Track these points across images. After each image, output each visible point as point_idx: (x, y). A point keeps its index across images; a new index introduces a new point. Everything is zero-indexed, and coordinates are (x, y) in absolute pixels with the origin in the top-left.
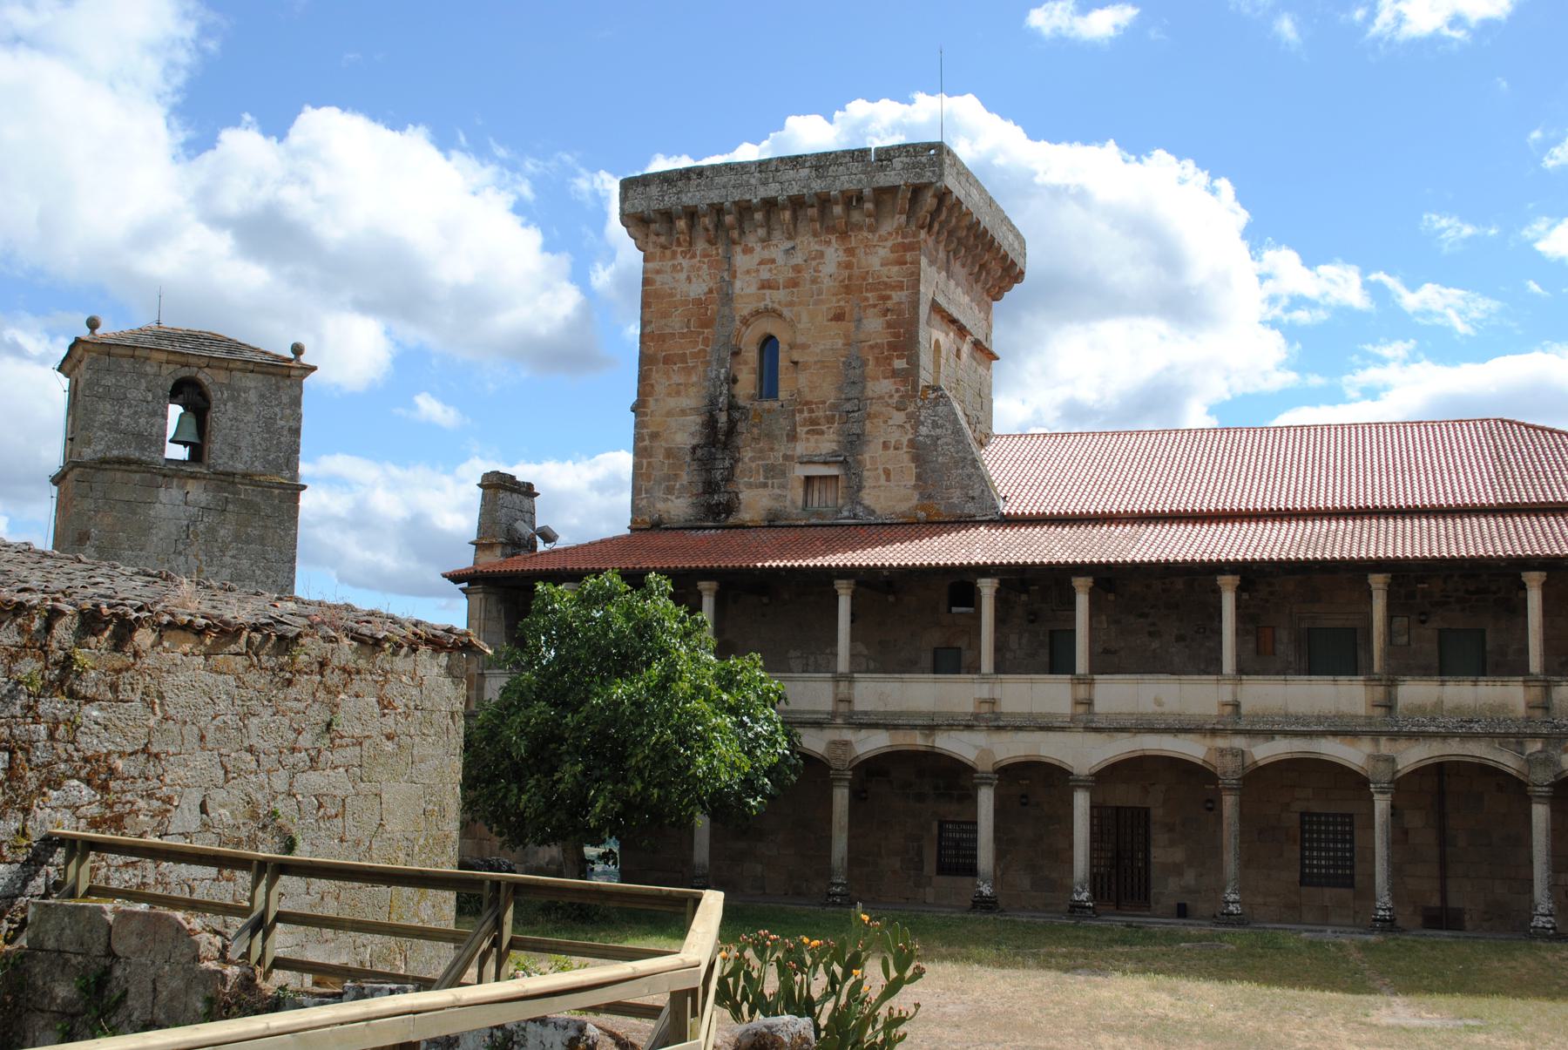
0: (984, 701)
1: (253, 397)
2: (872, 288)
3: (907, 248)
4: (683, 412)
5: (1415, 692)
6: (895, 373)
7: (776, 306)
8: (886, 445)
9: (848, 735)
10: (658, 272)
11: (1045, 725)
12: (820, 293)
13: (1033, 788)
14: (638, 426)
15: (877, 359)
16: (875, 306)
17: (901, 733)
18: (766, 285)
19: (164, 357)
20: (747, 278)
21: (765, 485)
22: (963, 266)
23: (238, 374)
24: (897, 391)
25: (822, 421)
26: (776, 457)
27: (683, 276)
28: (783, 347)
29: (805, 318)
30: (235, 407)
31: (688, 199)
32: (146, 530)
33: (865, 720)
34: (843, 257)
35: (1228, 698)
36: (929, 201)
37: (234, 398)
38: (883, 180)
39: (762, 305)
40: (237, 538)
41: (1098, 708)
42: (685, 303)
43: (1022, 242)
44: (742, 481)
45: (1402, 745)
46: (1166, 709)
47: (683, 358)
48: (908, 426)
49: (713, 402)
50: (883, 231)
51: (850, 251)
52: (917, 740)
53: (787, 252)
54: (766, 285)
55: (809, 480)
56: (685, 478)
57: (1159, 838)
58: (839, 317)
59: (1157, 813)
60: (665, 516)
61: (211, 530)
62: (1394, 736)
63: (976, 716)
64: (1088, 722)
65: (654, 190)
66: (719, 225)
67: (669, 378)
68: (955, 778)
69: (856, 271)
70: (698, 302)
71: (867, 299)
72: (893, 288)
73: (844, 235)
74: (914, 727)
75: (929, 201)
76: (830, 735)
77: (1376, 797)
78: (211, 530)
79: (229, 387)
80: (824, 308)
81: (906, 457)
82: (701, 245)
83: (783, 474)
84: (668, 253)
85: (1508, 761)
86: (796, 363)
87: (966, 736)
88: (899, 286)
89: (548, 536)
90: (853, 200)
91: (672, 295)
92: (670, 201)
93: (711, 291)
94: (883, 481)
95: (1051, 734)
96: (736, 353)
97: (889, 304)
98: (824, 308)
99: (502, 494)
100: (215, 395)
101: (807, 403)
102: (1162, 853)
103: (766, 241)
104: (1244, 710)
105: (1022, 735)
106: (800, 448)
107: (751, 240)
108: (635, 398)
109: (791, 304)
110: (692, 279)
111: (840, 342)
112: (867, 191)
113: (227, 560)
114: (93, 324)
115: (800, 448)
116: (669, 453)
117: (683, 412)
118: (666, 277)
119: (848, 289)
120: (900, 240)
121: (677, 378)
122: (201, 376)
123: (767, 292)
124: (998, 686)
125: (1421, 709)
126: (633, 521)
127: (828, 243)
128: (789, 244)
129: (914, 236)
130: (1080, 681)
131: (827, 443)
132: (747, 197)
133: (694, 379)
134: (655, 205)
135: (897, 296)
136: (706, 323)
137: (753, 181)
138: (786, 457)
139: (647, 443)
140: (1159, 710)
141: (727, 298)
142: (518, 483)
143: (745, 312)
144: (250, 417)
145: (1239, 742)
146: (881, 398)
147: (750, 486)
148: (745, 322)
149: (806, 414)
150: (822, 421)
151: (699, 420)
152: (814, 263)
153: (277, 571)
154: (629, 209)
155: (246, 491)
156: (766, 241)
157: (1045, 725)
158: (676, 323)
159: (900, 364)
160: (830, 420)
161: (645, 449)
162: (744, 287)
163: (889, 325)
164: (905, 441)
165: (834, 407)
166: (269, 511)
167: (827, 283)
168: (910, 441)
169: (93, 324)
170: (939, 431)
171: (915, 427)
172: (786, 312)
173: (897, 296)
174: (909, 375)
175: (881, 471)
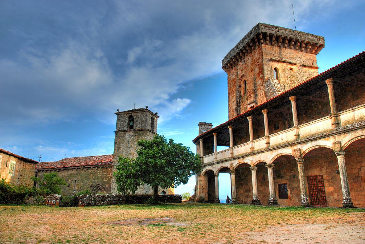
1: (139, 116)
2: (256, 61)
5: (346, 116)
6: (261, 78)
8: (261, 95)
9: (232, 162)
11: (260, 152)
13: (261, 167)
16: (256, 65)
18: (242, 70)
26: (245, 105)
32: (124, 141)
33: (236, 157)
35: (295, 133)
38: (251, 37)
45: (342, 136)
46: (284, 141)
48: (264, 89)
50: (257, 49)
51: (252, 56)
52: (241, 161)
57: (326, 184)
58: (252, 71)
59: (325, 176)
61: (133, 139)
62: (339, 133)
64: (269, 149)
70: (234, 79)
72: (258, 60)
77: (338, 157)
79: (136, 116)
81: (264, 96)
82: (234, 67)
97: (259, 63)
99: (201, 126)
100: (134, 117)
101: (249, 91)
102: (329, 189)
104: (301, 136)
107: (240, 63)
114: (118, 110)
115: (249, 102)
119: (252, 64)
120: (259, 48)
121: (232, 95)
122: (132, 115)
124: (254, 144)
125: (348, 122)
127: (249, 56)
134: (225, 63)
135: (260, 61)
136: (235, 83)
138: (247, 105)
140: (282, 141)
145: (299, 146)
148: (241, 79)
151: (235, 102)
155: (139, 132)
156: (241, 61)
157: (260, 152)
159: (261, 76)
163: (259, 68)
165: (253, 90)
169: (118, 110)
172: (245, 74)
174: (263, 78)
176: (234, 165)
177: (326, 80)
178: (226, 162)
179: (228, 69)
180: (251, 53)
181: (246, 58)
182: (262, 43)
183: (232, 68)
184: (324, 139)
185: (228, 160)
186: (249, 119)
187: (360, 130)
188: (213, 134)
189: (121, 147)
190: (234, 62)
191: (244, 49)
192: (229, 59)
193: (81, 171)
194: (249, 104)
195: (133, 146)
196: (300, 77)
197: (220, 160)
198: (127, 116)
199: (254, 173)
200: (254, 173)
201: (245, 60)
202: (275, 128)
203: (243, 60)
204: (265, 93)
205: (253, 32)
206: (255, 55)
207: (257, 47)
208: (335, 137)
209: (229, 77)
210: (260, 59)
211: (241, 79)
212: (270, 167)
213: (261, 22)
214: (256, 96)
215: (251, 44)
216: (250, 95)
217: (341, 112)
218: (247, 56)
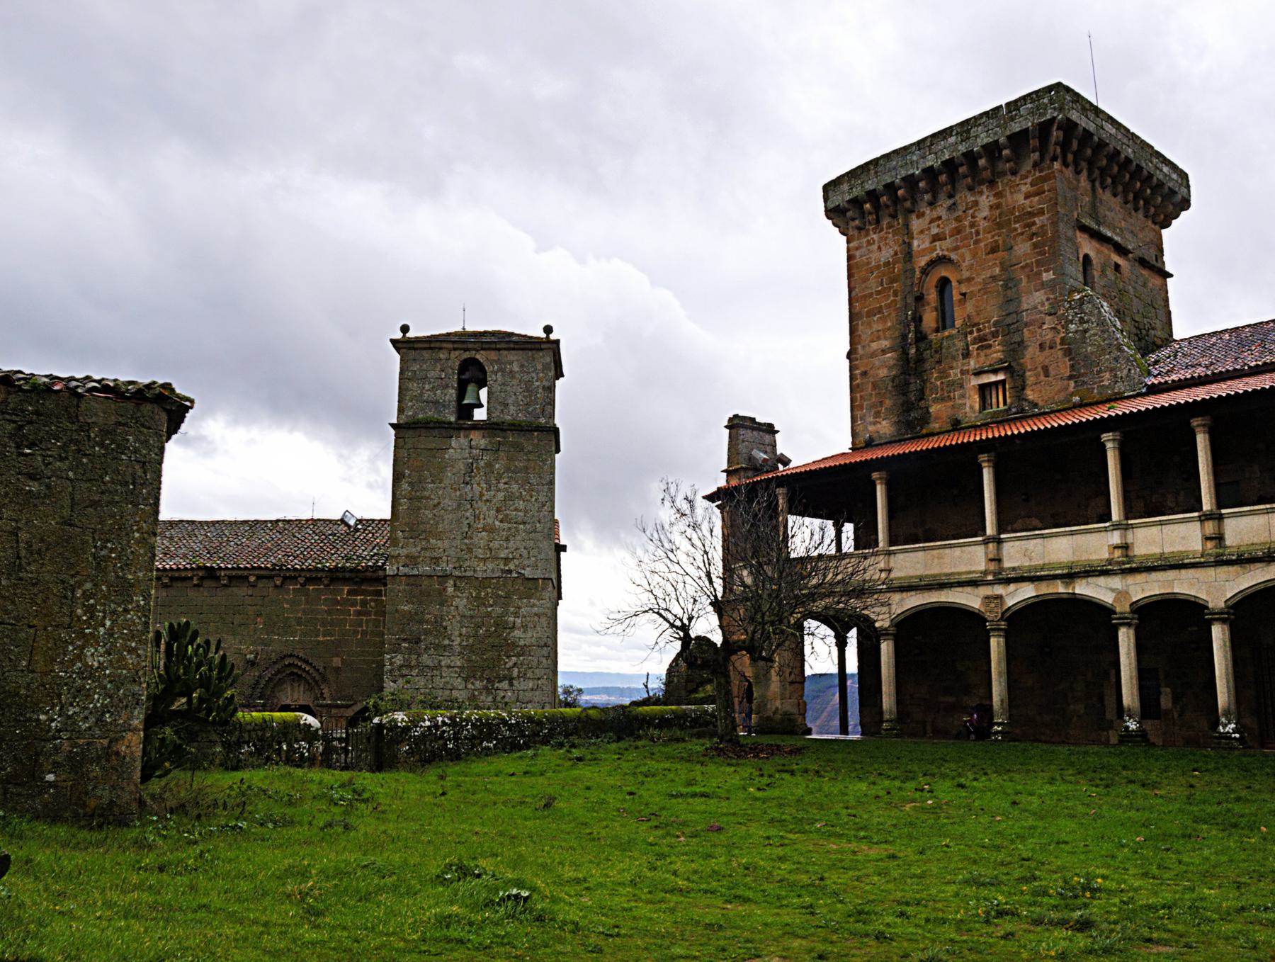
0: (1116, 547)
1: (516, 368)
3: (1045, 179)
4: (884, 352)
6: (1043, 285)
8: (1042, 346)
9: (999, 590)
10: (857, 249)
12: (978, 233)
13: (1171, 623)
15: (1028, 277)
16: (1022, 234)
17: (1044, 584)
18: (936, 238)
19: (451, 346)
20: (922, 236)
22: (1115, 195)
23: (505, 352)
24: (1048, 299)
25: (989, 337)
26: (955, 374)
27: (875, 247)
28: (954, 284)
30: (503, 376)
31: (870, 186)
32: (442, 469)
34: (993, 200)
36: (1056, 134)
37: (502, 370)
38: (1016, 127)
39: (934, 255)
40: (508, 470)
41: (1229, 541)
42: (878, 267)
43: (1184, 176)
47: (880, 310)
49: (904, 337)
50: (1023, 172)
51: (999, 195)
52: (1060, 588)
53: (949, 208)
54: (936, 238)
55: (984, 389)
56: (888, 403)
58: (994, 249)
60: (875, 435)
63: (1110, 562)
64: (1221, 557)
65: (845, 187)
66: (896, 201)
67: (871, 327)
68: (1098, 618)
70: (887, 264)
71: (1016, 229)
73: (992, 183)
74: (1055, 577)
78: (489, 465)
80: (982, 245)
81: (1060, 354)
83: (962, 386)
84: (863, 232)
86: (964, 295)
87: (1102, 580)
88: (1041, 212)
89: (786, 462)
90: (992, 150)
91: (869, 263)
92: (857, 192)
93: (896, 254)
94: (1042, 377)
95: (1183, 571)
96: (920, 299)
97: (1034, 229)
101: (975, 325)
103: (931, 204)
105: (1155, 576)
108: (848, 348)
109: (956, 249)
110: (883, 250)
111: (997, 270)
112: (1002, 140)
113: (501, 486)
114: (405, 329)
117: (884, 352)
118: (863, 250)
121: (876, 327)
122: (478, 357)
123: (937, 243)
126: (853, 443)
127: (981, 193)
128: (950, 202)
129: (1049, 168)
131: (997, 352)
132: (911, 172)
134: (848, 197)
137: (915, 158)
141: (909, 255)
142: (760, 424)
143: (923, 264)
144: (515, 382)
146: (1036, 308)
147: (936, 401)
150: (989, 337)
153: (538, 492)
154: (831, 206)
156: (931, 204)
158: (873, 285)
159: (1047, 276)
160: (995, 335)
161: (858, 385)
163: (1035, 246)
166: (530, 448)
167: (983, 224)
168: (1063, 340)
169: (405, 329)
170: (1085, 326)
171: (1065, 327)
172: (953, 256)
175: (1039, 369)
176: (1010, 602)
178: (960, 589)
179: (857, 222)
180: (992, 183)
181: (964, 197)
182: (1054, 159)
183: (878, 221)
185: (974, 583)
189: (426, 493)
193: (192, 593)
194: (978, 373)
195: (487, 496)
196: (1135, 300)
197: (916, 577)
198: (456, 358)
199: (1126, 639)
204: (1063, 341)
207: (1027, 166)
209: (858, 253)
211: (925, 271)
212: (1223, 621)
213: (1065, 83)
215: (1006, 152)
216: (982, 339)
218: (970, 189)
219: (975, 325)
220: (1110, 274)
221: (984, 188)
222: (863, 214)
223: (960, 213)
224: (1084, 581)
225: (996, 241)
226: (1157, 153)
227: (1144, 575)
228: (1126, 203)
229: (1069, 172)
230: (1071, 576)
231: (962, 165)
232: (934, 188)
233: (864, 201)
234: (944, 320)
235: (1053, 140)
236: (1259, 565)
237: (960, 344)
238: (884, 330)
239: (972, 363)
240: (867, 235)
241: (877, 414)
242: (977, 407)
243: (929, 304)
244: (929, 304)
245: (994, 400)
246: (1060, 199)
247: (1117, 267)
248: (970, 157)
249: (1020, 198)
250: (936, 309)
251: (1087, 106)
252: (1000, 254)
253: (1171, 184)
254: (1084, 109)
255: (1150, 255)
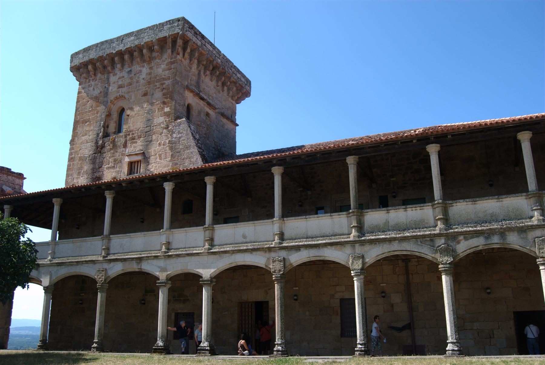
2: (158, 81)
3: (172, 63)
7: (123, 94)
9: (106, 266)
13: (185, 286)
14: (71, 149)
15: (158, 109)
16: (159, 88)
18: (120, 87)
21: (113, 167)
25: (137, 137)
27: (92, 88)
29: (133, 97)
34: (149, 71)
36: (180, 42)
38: (161, 35)
44: (105, 167)
45: (367, 247)
50: (164, 59)
51: (151, 68)
52: (134, 267)
54: (120, 87)
65: (81, 56)
69: (153, 75)
71: (156, 86)
75: (180, 42)
76: (98, 266)
80: (140, 92)
81: (167, 148)
82: (99, 75)
84: (88, 80)
85: (426, 252)
87: (155, 262)
88: (169, 78)
90: (150, 47)
93: (101, 92)
94: (158, 160)
95: (193, 257)
97: (164, 86)
98: (140, 92)
101: (130, 131)
106: (128, 151)
107: (117, 71)
109: (128, 92)
116: (81, 159)
119: (149, 83)
120: (170, 60)
123: (120, 89)
127: (143, 66)
128: (129, 69)
130: (206, 229)
132: (112, 51)
133: (92, 128)
135: (167, 82)
139: (73, 156)
142: (14, 173)
149: (131, 136)
152: (138, 75)
162: (113, 88)
163: (164, 95)
164: (167, 141)
167: (142, 81)
168: (169, 141)
170: (180, 135)
172: (127, 97)
173: (167, 82)
177: (349, 157)
178: (86, 265)
180: (149, 62)
181: (136, 68)
182: (179, 54)
183: (95, 75)
184: (333, 248)
186: (168, 187)
187: (397, 241)
188: (54, 200)
190: (105, 67)
191: (136, 49)
192: (93, 55)
199: (162, 297)
200: (162, 297)
201: (131, 70)
202: (226, 215)
203: (127, 69)
204: (170, 142)
205: (165, 28)
206: (157, 68)
208: (354, 246)
210: (169, 79)
214: (149, 142)
217: (368, 211)
219: (130, 131)
220: (203, 117)
221: (145, 64)
222: (88, 72)
223: (133, 75)
224: (147, 262)
225: (147, 91)
226: (235, 66)
227: (174, 259)
228: (218, 86)
229: (186, 62)
230: (140, 260)
231: (135, 51)
232: (122, 60)
233: (90, 67)
234: (119, 130)
235: (178, 44)
236: (227, 255)
237: (123, 140)
238: (89, 131)
239: (127, 150)
240: (89, 82)
241: (79, 173)
242: (126, 173)
243: (113, 119)
244: (113, 119)
245: (136, 170)
246: (178, 73)
247: (207, 114)
248: (140, 49)
249: (160, 71)
250: (116, 123)
251: (198, 33)
252: (147, 97)
253: (241, 83)
254: (195, 33)
255: (228, 113)
